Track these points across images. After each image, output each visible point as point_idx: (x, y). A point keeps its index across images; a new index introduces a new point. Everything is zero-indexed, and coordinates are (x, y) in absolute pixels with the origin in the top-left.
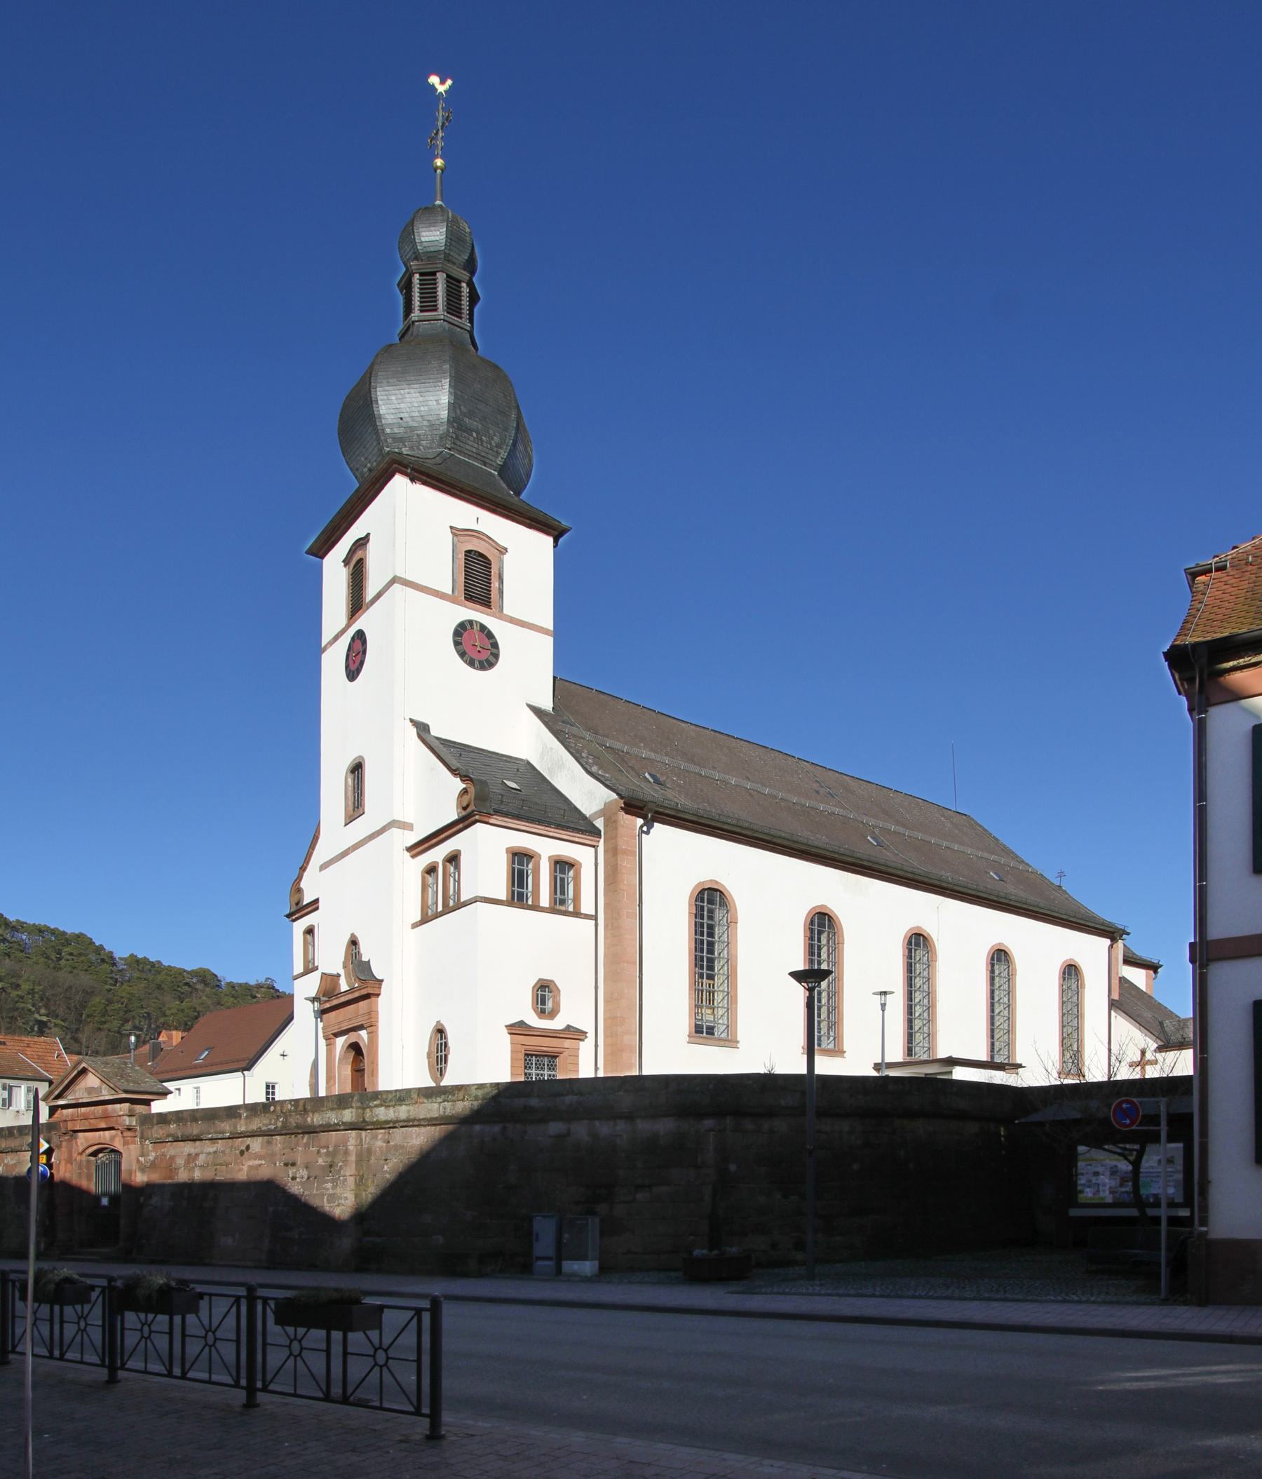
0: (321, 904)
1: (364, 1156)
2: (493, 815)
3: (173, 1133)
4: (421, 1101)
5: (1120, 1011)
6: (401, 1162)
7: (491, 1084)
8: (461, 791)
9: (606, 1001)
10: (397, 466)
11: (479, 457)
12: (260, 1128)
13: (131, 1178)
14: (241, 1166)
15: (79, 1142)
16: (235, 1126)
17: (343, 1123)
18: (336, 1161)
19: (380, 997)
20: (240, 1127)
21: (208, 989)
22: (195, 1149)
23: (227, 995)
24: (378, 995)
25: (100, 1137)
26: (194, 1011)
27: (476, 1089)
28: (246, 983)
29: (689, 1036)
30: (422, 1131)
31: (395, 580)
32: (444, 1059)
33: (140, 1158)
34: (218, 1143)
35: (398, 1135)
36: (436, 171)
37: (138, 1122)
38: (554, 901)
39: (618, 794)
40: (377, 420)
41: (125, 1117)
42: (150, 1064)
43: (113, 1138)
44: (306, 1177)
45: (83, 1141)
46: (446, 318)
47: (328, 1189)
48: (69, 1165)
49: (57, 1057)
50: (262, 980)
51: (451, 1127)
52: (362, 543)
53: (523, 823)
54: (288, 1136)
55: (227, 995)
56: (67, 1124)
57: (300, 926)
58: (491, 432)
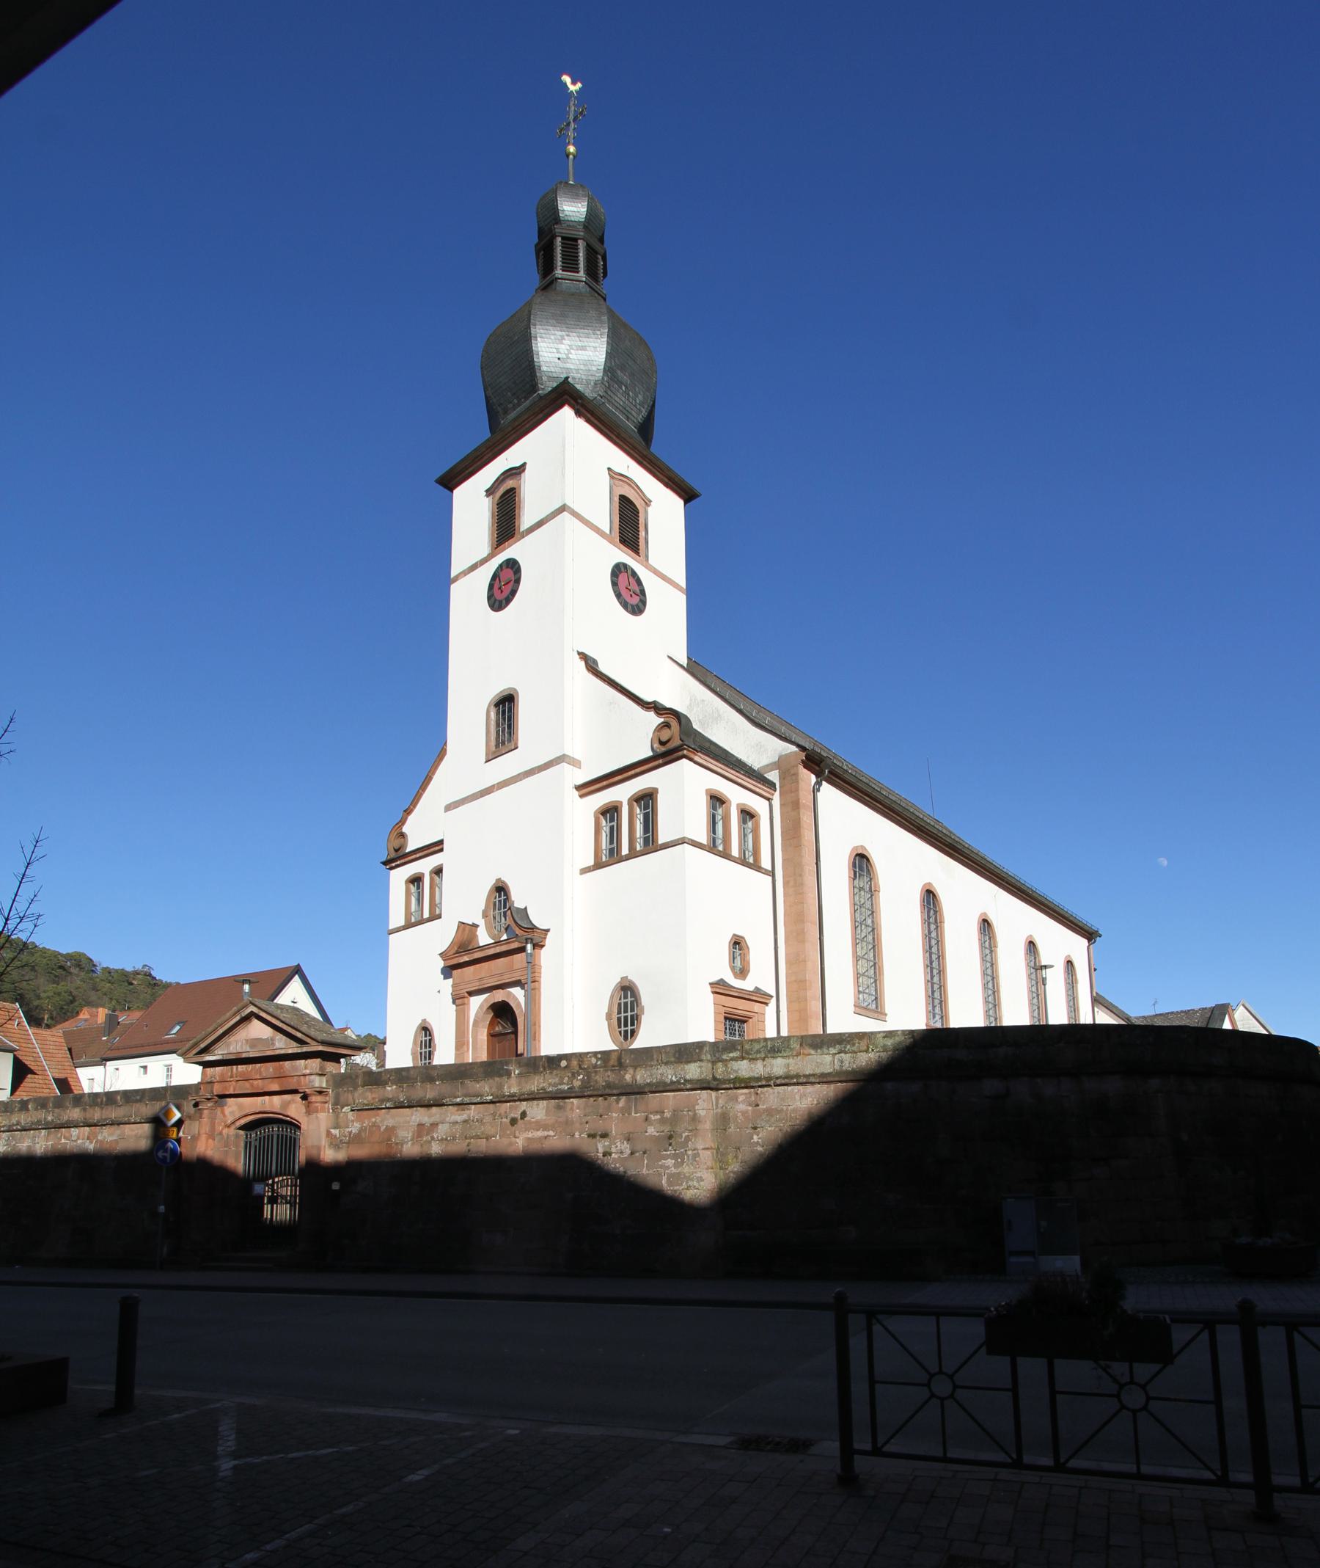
0: (445, 846)
1: (723, 1120)
2: (697, 751)
3: (391, 1096)
4: (806, 1052)
5: (1103, 1007)
6: (780, 1130)
7: (903, 1031)
8: (659, 725)
9: (788, 962)
10: (568, 398)
11: (624, 411)
12: (543, 1089)
13: (319, 1155)
14: (514, 1139)
15: (227, 1110)
16: (500, 1087)
17: (685, 1080)
18: (678, 1129)
19: (544, 949)
20: (509, 1087)
21: (83, 974)
22: (430, 1117)
23: (102, 980)
24: (543, 946)
25: (263, 1104)
26: (69, 995)
27: (884, 1037)
28: (123, 970)
29: (855, 1006)
30: (808, 1091)
31: (563, 509)
32: (635, 1020)
33: (332, 1131)
34: (470, 1109)
35: (771, 1096)
36: (568, 156)
37: (331, 1083)
38: (743, 851)
39: (798, 746)
40: (535, 356)
41: (313, 1077)
42: (105, 1038)
43: (286, 1105)
44: (628, 1152)
45: (235, 1108)
46: (587, 281)
47: (668, 1167)
48: (210, 1141)
49: (17, 1025)
50: (139, 967)
51: (862, 1083)
52: (517, 472)
53: (720, 765)
54: (592, 1099)
55: (102, 980)
56: (212, 1087)
57: (399, 876)
58: (637, 389)
